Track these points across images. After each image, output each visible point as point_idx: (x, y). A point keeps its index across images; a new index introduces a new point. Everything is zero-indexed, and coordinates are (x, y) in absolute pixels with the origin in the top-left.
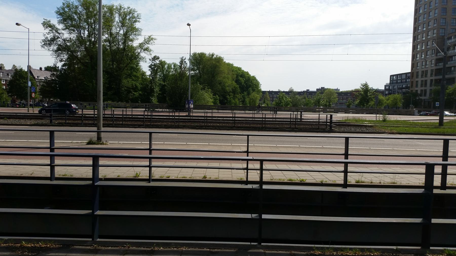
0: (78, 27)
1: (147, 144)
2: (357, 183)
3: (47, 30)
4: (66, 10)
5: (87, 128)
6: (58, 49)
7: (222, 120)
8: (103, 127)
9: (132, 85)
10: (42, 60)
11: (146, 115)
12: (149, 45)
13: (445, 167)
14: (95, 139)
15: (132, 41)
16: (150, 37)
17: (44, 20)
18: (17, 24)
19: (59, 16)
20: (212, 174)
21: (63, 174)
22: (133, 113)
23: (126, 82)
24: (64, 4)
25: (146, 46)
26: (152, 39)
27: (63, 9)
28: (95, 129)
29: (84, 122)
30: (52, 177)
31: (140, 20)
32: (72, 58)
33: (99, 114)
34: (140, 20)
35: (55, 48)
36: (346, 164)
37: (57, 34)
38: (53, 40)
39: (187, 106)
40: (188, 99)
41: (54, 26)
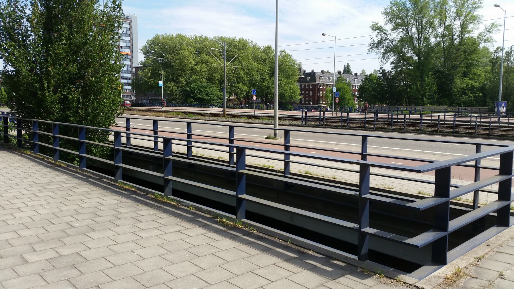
0: (405, 26)
1: (497, 160)
2: (420, 193)
3: (376, 32)
4: (395, 9)
5: (365, 132)
6: (386, 52)
7: (507, 127)
8: (279, 125)
9: (467, 85)
10: (371, 64)
11: (479, 122)
12: (491, 35)
13: (128, 134)
14: (272, 136)
15: (469, 32)
16: (493, 24)
17: (372, 23)
18: (323, 34)
19: (385, 17)
20: (315, 171)
21: (315, 173)
22: (446, 119)
23: (459, 83)
24: (391, 3)
25: (488, 35)
26: (496, 26)
27: (391, 8)
28: (272, 127)
29: (440, 130)
30: (286, 171)
31: (482, 5)
32: (402, 57)
33: (275, 114)
34: (482, 5)
35: (382, 50)
36: (287, 155)
37: (384, 36)
38: (380, 42)
39: (496, 110)
40: (498, 100)
41: (381, 27)
